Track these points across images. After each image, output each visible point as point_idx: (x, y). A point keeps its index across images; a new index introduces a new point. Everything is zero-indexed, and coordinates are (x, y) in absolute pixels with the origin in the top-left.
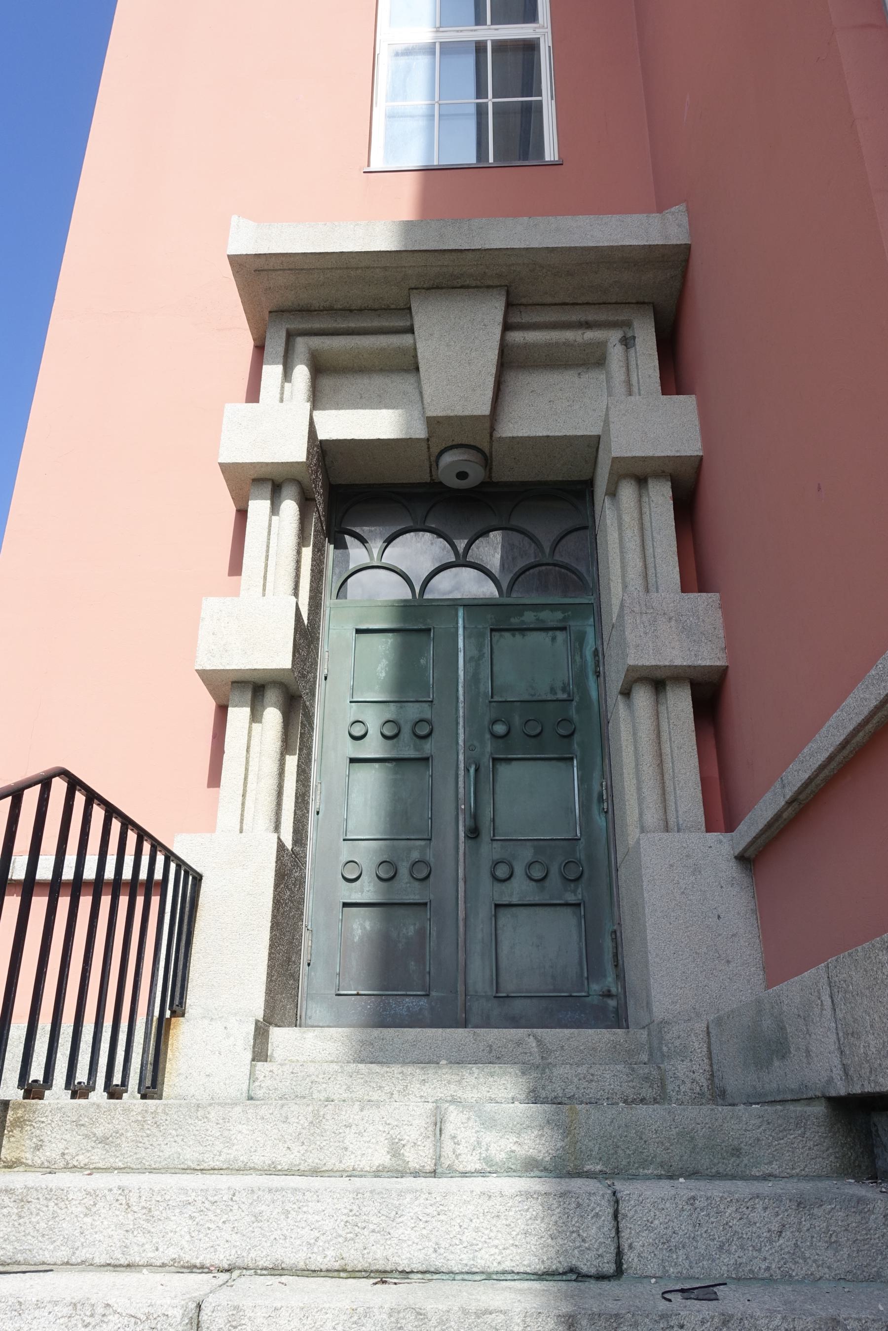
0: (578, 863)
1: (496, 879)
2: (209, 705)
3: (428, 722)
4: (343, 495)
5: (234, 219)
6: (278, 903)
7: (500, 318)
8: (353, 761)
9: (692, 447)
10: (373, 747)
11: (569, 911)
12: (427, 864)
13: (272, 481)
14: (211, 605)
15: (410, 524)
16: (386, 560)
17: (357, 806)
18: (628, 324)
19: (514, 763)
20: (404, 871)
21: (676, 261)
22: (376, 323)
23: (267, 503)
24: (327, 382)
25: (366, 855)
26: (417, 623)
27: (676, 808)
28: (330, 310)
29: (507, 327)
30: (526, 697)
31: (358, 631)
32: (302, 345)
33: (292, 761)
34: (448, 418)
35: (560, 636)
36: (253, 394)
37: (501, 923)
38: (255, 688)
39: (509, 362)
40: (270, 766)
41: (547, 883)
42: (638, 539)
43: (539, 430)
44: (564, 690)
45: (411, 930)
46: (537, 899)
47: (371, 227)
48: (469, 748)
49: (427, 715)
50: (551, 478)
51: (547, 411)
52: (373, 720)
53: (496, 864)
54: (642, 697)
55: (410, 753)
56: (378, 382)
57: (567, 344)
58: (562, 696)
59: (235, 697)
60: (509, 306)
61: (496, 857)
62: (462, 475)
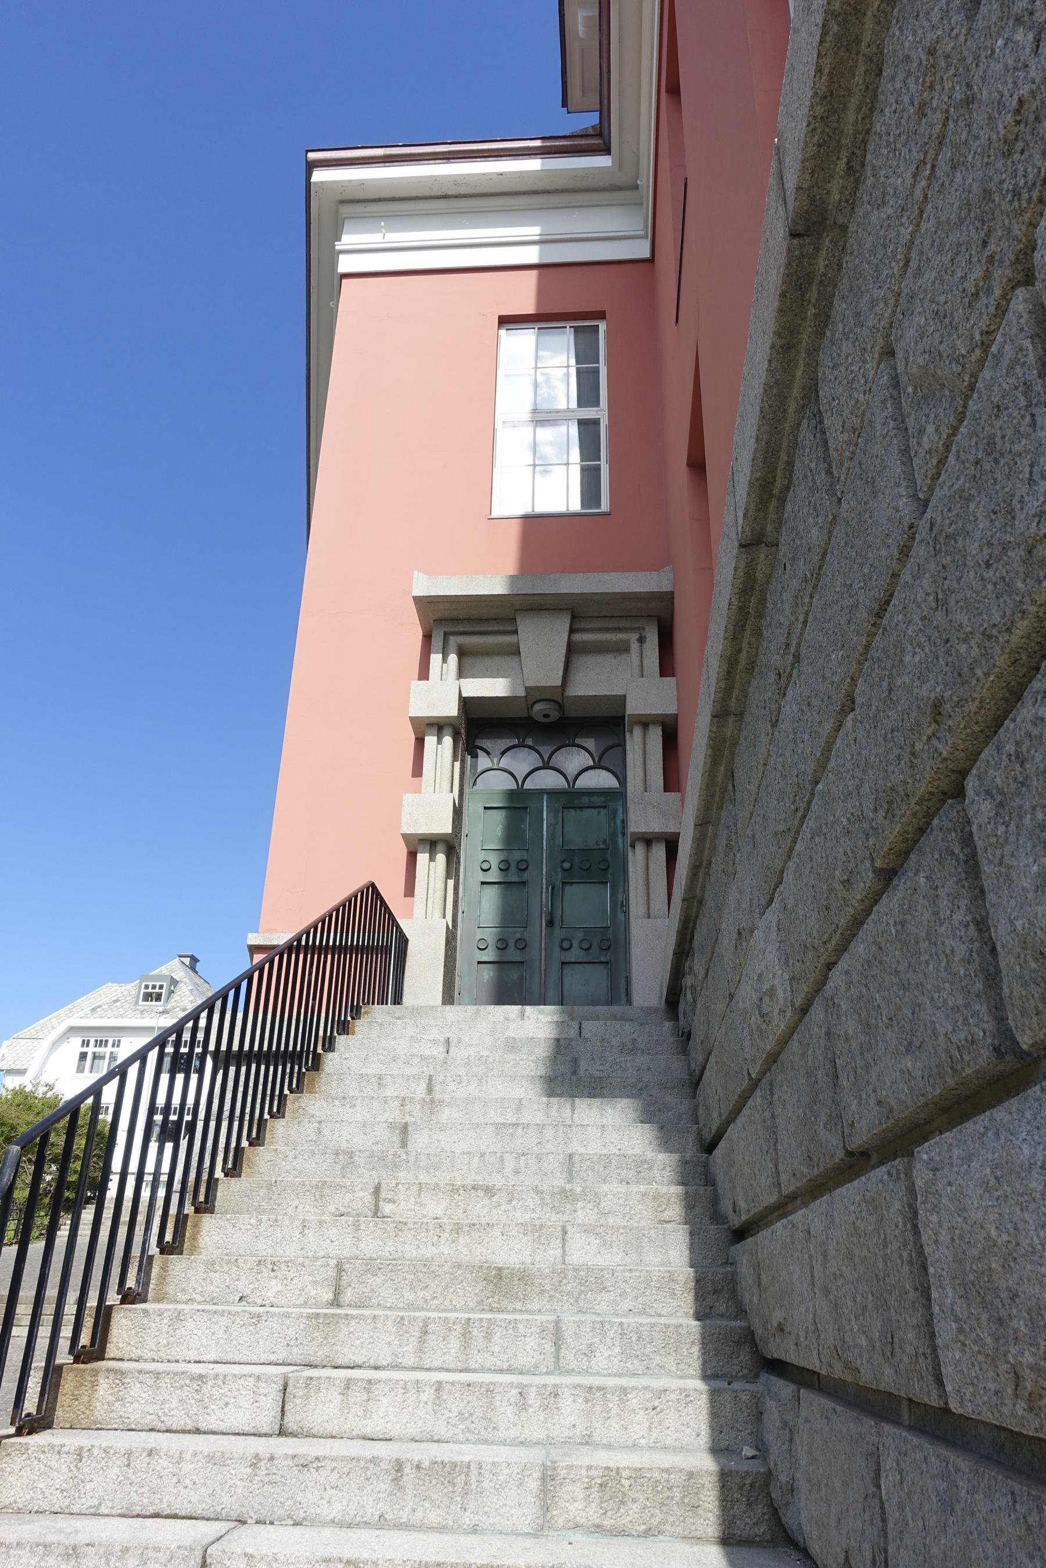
0: (608, 940)
1: (562, 949)
2: (403, 851)
3: (525, 861)
4: (476, 727)
5: (416, 573)
6: (446, 956)
7: (567, 628)
8: (483, 883)
9: (671, 709)
10: (494, 876)
11: (602, 966)
12: (525, 940)
13: (439, 726)
14: (408, 798)
15: (516, 742)
16: (501, 765)
17: (486, 908)
18: (644, 629)
19: (574, 886)
20: (511, 944)
21: (668, 599)
22: (496, 628)
23: (435, 738)
24: (467, 661)
25: (490, 935)
26: (518, 804)
27: (843, 948)
28: (469, 620)
29: (572, 631)
30: (582, 847)
31: (485, 808)
32: (453, 641)
33: (451, 883)
34: (537, 687)
35: (603, 811)
36: (424, 674)
37: (565, 972)
38: (432, 843)
39: (572, 650)
40: (440, 885)
41: (591, 951)
42: (641, 760)
43: (591, 692)
44: (604, 842)
45: (515, 976)
46: (585, 960)
47: (491, 581)
48: (549, 876)
49: (525, 858)
50: (600, 715)
51: (595, 681)
52: (494, 860)
53: (563, 940)
54: (640, 848)
55: (516, 879)
56: (497, 660)
57: (607, 641)
58: (602, 846)
59: (420, 848)
60: (574, 618)
61: (563, 937)
62: (546, 716)
